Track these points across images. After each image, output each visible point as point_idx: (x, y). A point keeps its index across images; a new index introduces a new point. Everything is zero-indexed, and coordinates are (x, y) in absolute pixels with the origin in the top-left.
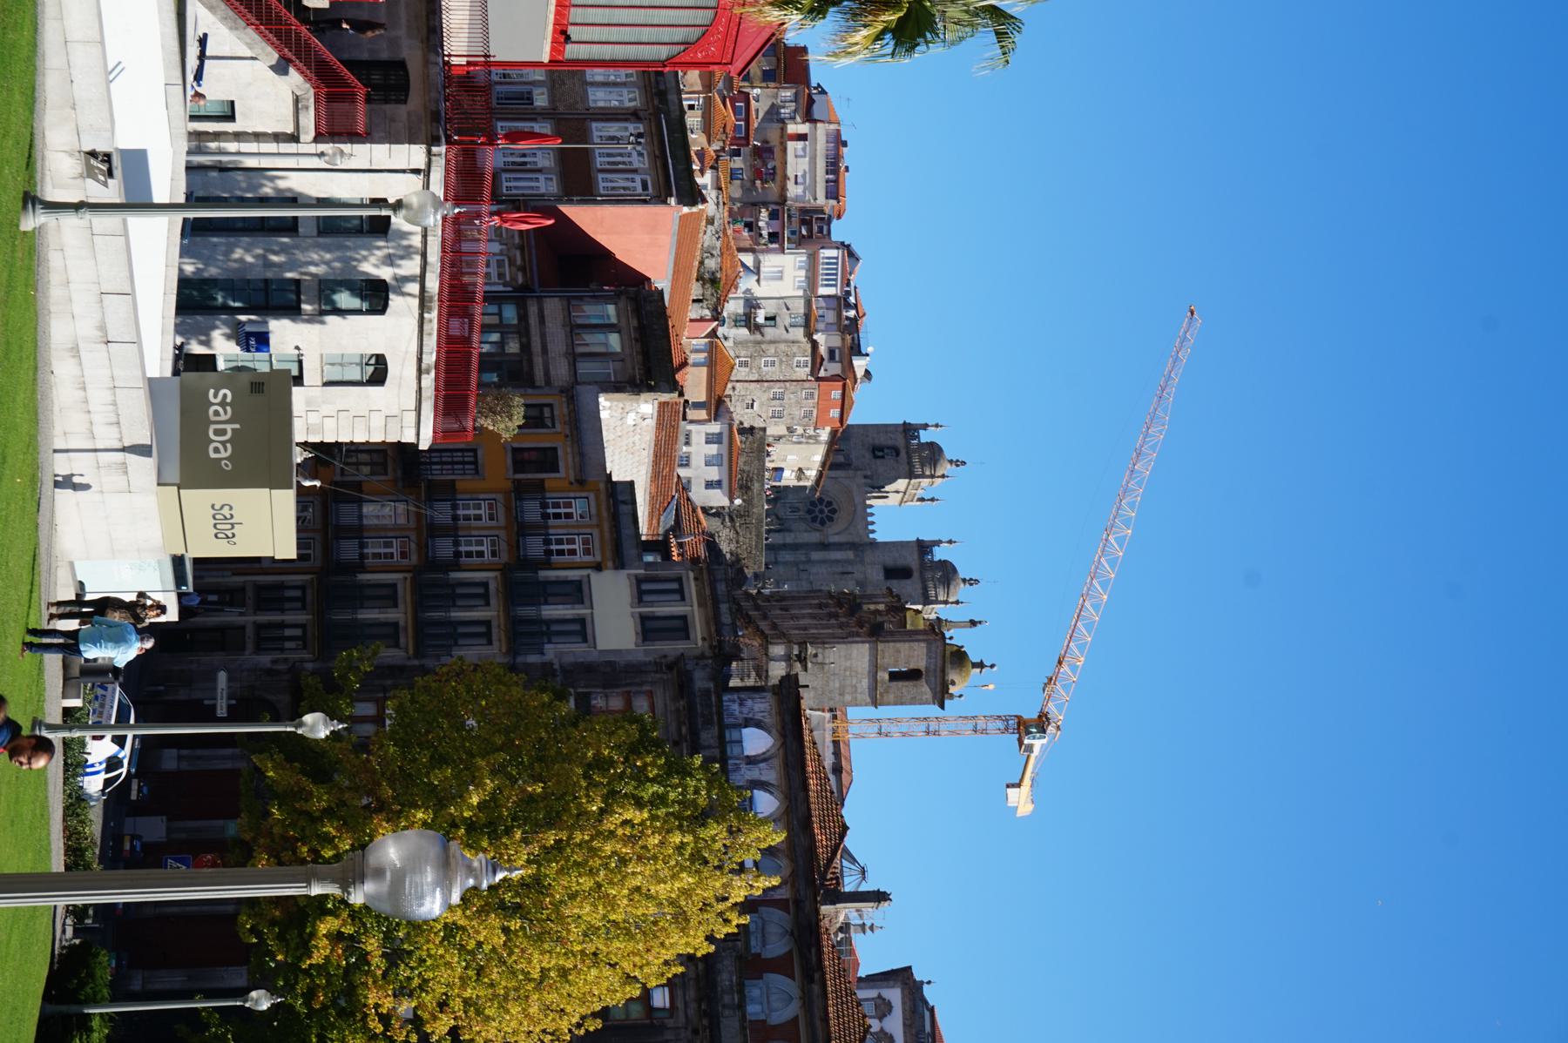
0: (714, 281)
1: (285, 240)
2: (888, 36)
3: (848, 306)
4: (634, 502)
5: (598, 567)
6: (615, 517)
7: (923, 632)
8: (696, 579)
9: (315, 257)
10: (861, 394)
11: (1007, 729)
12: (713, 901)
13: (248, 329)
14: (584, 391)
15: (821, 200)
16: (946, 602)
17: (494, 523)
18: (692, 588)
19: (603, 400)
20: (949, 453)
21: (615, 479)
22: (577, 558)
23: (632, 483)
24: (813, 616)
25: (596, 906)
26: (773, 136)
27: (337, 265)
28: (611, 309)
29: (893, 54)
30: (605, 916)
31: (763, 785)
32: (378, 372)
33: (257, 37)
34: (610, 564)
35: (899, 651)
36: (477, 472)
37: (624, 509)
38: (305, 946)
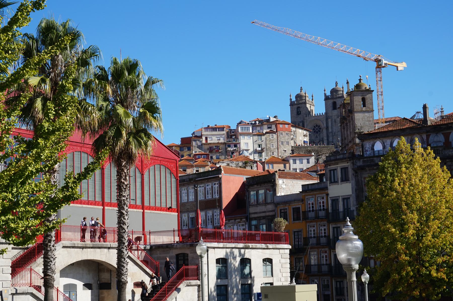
0: (246, 163)
1: (229, 288)
2: (154, 115)
3: (255, 123)
4: (308, 185)
5: (327, 195)
6: (313, 190)
7: (351, 97)
8: (330, 166)
9: (234, 280)
10: (281, 119)
11: (380, 71)
12: (423, 158)
13: (256, 299)
14: (276, 200)
15: (224, 132)
16: (343, 91)
18: (333, 167)
19: (279, 194)
20: (298, 92)
21: (301, 191)
23: (303, 186)
24: (347, 131)
25: (425, 193)
26: (206, 147)
27: (236, 273)
28: (252, 193)
29: (159, 114)
30: (428, 190)
31: (391, 144)
32: (268, 261)
33: (169, 297)
34: (326, 191)
35: (357, 105)
36: (300, 231)
37: (310, 187)
38: (442, 280)
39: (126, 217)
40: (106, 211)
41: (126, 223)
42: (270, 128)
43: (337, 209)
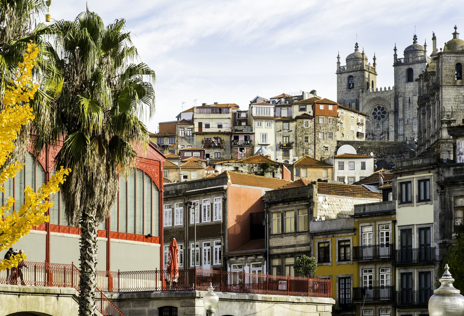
4: (364, 205)
5: (395, 222)
8: (401, 176)
10: (322, 95)
16: (425, 51)
17: (373, 270)
22: (390, 232)
34: (393, 216)
36: (350, 278)
37: (367, 210)
39: (93, 250)
40: (51, 239)
41: (94, 259)
42: (304, 109)
43: (409, 244)
